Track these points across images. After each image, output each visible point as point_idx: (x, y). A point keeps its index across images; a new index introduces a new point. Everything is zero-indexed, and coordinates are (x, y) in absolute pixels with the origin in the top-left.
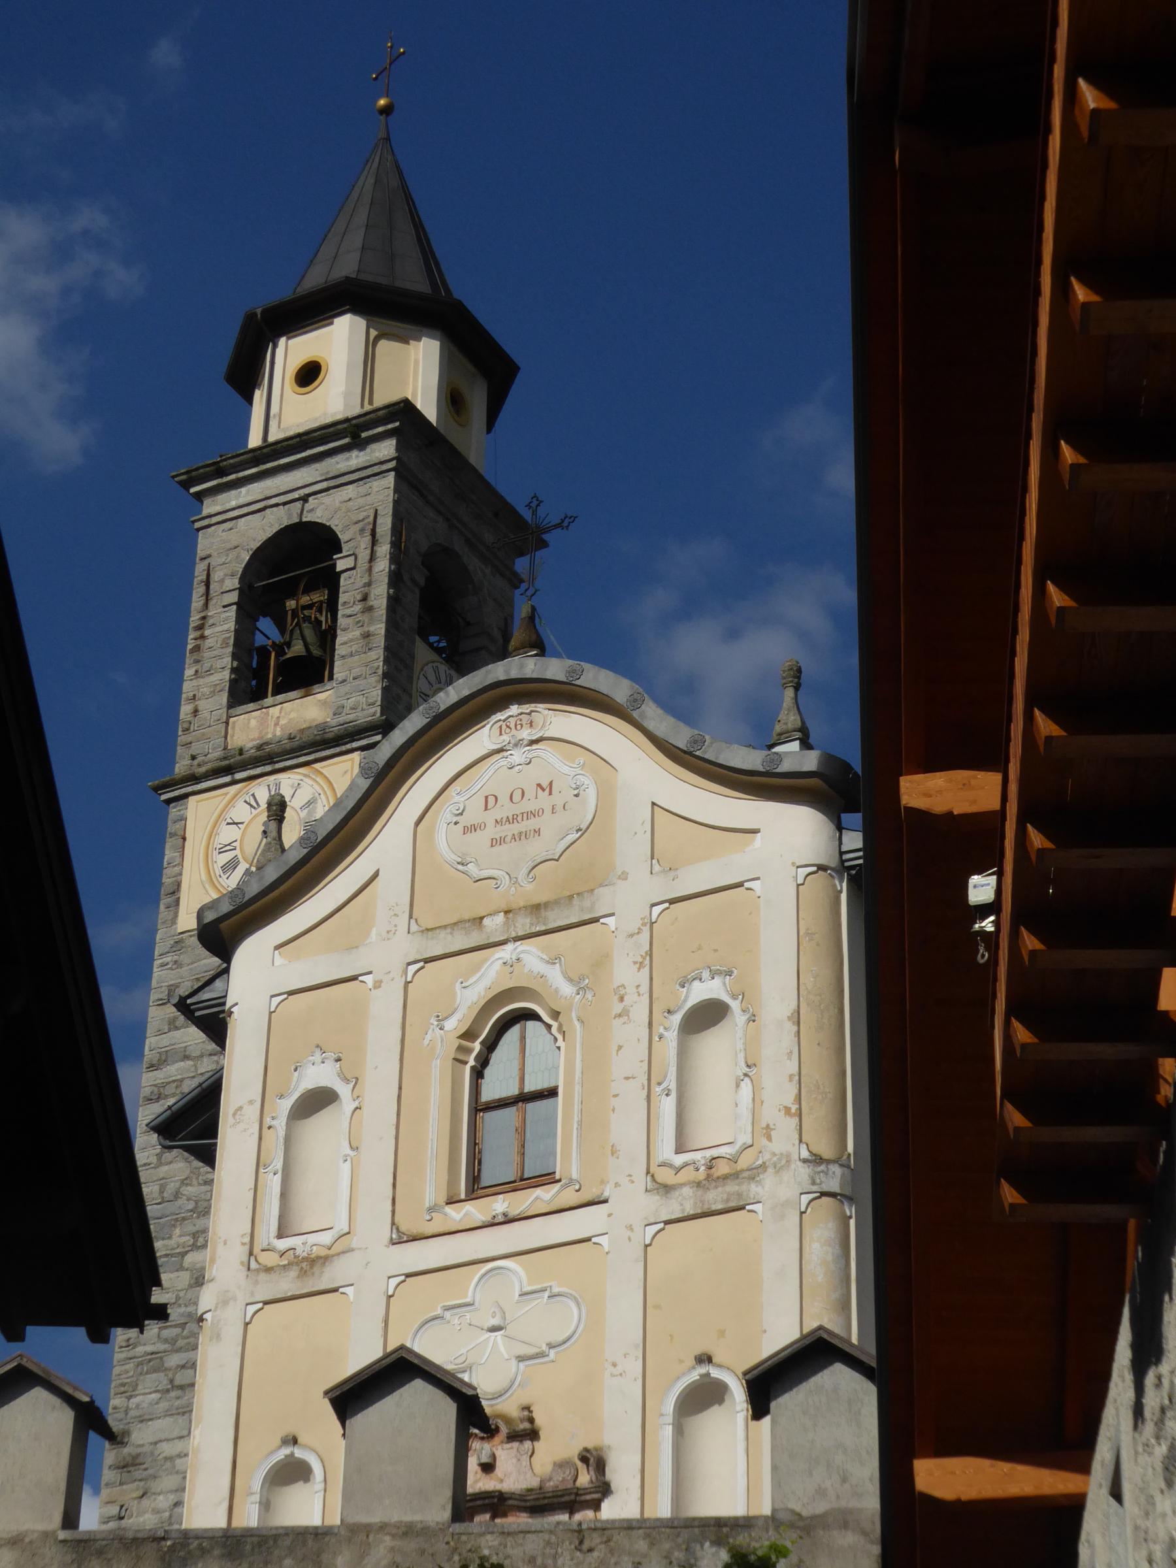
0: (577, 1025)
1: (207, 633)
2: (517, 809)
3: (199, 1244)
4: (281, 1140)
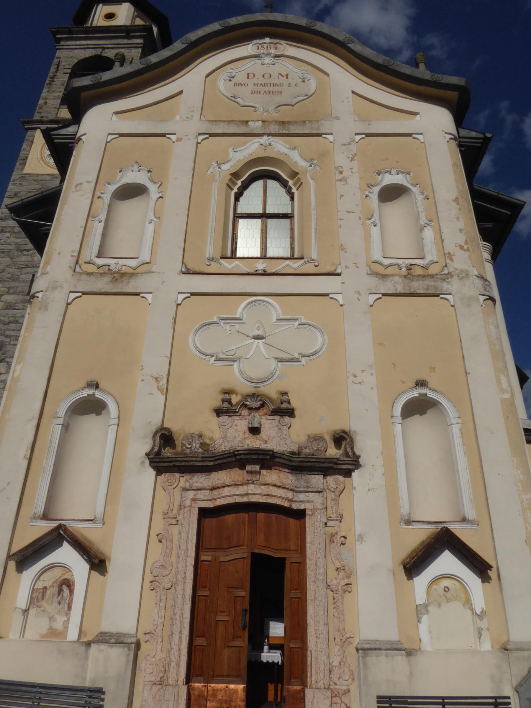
0: (312, 182)
1: (55, 80)
2: (268, 81)
3: (10, 292)
4: (106, 206)
